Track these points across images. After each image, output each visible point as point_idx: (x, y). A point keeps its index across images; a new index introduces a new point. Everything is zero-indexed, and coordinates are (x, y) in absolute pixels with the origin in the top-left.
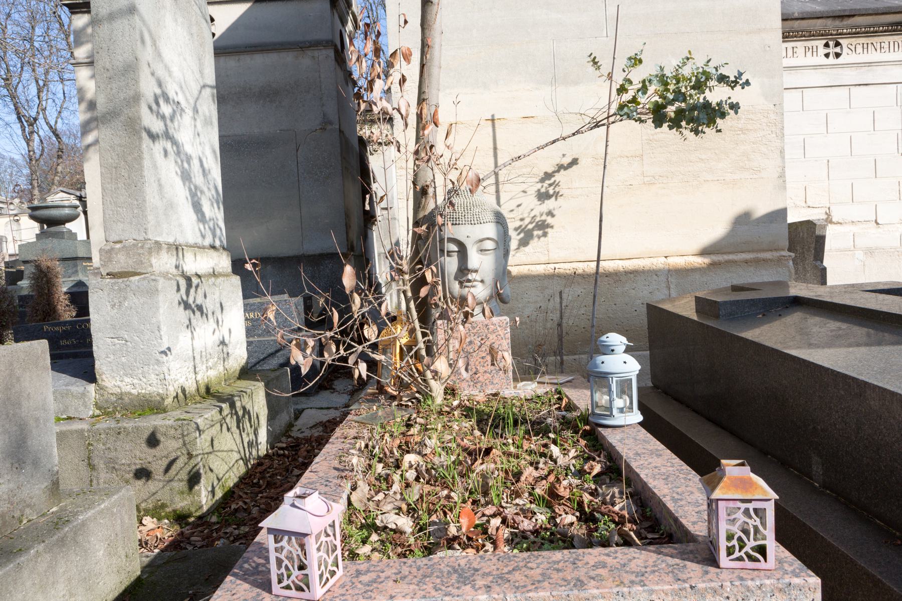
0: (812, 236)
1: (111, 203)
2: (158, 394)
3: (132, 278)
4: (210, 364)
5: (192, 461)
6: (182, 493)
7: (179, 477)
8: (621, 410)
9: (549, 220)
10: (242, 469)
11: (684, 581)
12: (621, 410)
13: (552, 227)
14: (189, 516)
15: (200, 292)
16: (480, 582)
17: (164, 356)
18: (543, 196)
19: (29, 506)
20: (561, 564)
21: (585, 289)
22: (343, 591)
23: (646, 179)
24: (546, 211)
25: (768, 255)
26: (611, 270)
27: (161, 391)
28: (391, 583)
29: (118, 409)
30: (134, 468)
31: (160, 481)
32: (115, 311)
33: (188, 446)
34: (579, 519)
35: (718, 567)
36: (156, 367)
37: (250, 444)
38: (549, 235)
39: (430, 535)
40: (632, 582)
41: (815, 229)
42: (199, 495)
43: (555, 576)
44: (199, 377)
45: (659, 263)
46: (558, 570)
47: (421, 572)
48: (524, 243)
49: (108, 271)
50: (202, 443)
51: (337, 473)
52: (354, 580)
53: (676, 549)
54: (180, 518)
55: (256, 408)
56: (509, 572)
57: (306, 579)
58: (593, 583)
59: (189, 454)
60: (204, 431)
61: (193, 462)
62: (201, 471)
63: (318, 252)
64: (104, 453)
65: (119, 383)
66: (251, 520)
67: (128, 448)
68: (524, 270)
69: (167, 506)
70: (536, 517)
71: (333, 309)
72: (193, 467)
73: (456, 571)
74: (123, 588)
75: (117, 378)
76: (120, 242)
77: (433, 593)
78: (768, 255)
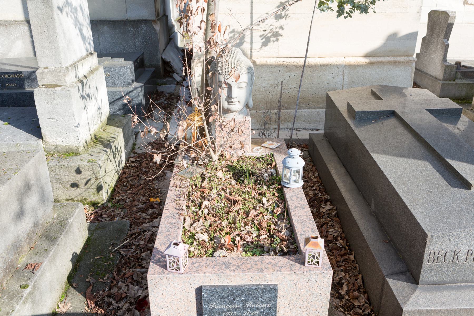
0: (446, 23)
1: (39, 47)
2: (76, 146)
3: (56, 88)
4: (95, 123)
5: (98, 181)
6: (94, 194)
7: (92, 187)
8: (295, 181)
9: (281, 32)
10: (117, 177)
11: (293, 271)
12: (295, 181)
13: (282, 36)
14: (98, 203)
15: (88, 86)
16: (232, 268)
17: (77, 128)
18: (278, 17)
19: (48, 217)
20: (257, 262)
21: (297, 74)
22: (189, 270)
24: (279, 26)
25: (401, 59)
26: (313, 64)
27: (77, 145)
28: (204, 267)
29: (56, 152)
30: (70, 183)
31: (83, 188)
32: (49, 105)
33: (96, 174)
34: (268, 236)
35: (305, 266)
36: (73, 133)
37: (119, 163)
38: (280, 41)
39: (214, 243)
40: (278, 270)
41: (448, 18)
42: (102, 195)
43: (255, 267)
44: (91, 132)
45: (340, 61)
46: (256, 265)
47: (213, 263)
48: (265, 44)
49: (42, 84)
50: (102, 172)
51: (177, 211)
52: (192, 266)
53: (294, 257)
54: (94, 204)
55: (120, 144)
56: (241, 265)
57: (179, 268)
58: (266, 270)
59: (96, 177)
60: (102, 167)
61: (98, 181)
62: (103, 185)
63: (136, 18)
64: (55, 176)
65: (55, 140)
66: (127, 206)
67: (66, 174)
68: (263, 61)
69: (87, 199)
70: (253, 235)
71: (167, 122)
72: (99, 183)
73: (224, 263)
74: (84, 243)
75: (54, 138)
76: (47, 68)
77: (218, 272)
78: (401, 59)
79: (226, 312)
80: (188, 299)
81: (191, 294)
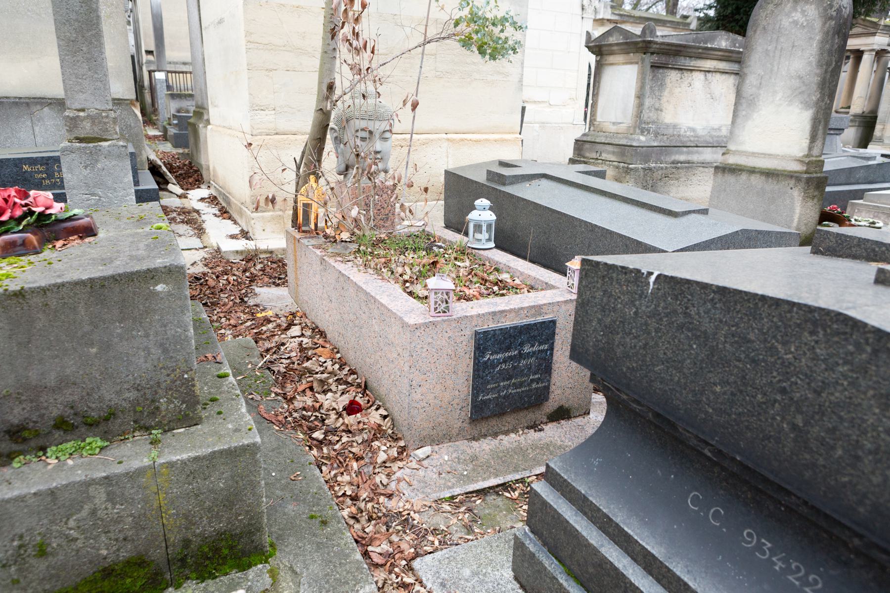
23: (438, 73)
76: (83, 110)
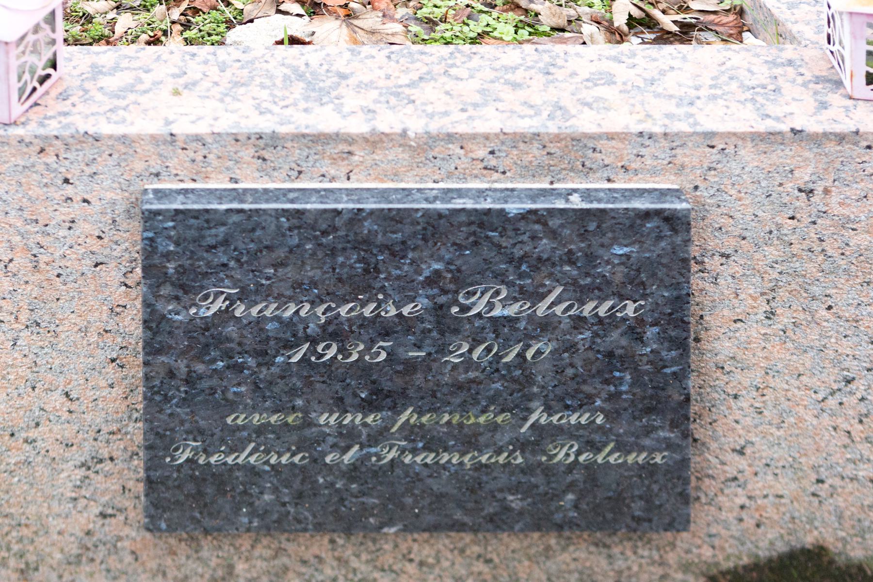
46: (515, 86)
47: (228, 74)
56: (411, 85)
73: (301, 77)
79: (314, 342)
80: (43, 258)
81: (63, 232)
